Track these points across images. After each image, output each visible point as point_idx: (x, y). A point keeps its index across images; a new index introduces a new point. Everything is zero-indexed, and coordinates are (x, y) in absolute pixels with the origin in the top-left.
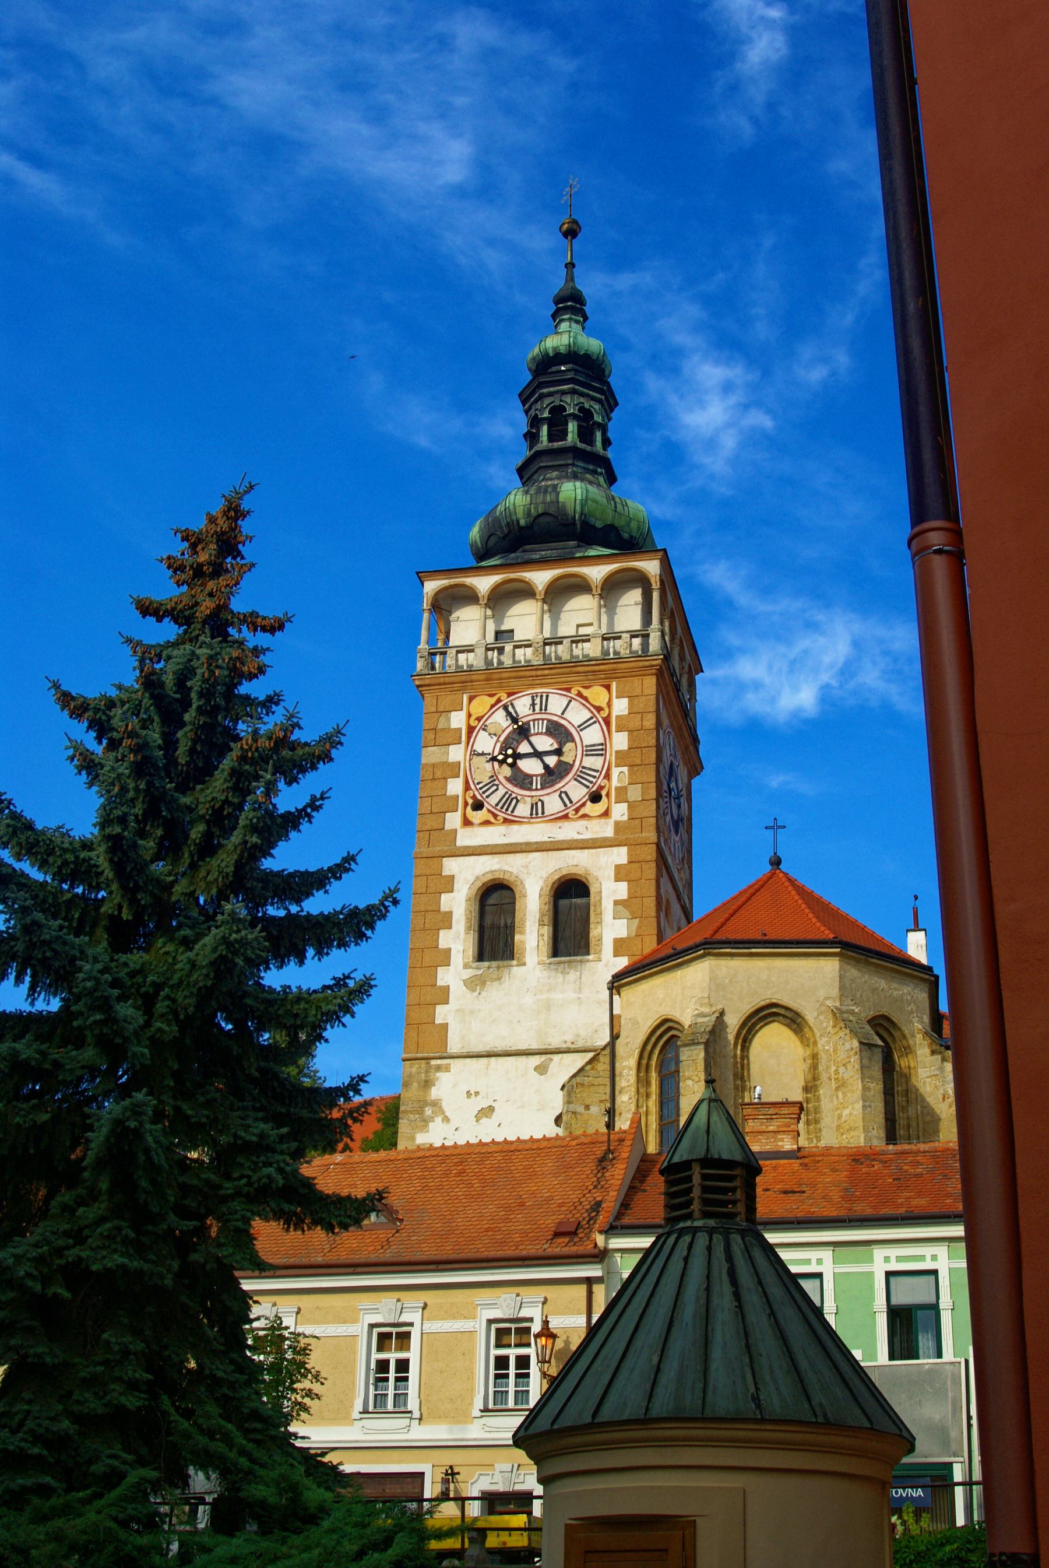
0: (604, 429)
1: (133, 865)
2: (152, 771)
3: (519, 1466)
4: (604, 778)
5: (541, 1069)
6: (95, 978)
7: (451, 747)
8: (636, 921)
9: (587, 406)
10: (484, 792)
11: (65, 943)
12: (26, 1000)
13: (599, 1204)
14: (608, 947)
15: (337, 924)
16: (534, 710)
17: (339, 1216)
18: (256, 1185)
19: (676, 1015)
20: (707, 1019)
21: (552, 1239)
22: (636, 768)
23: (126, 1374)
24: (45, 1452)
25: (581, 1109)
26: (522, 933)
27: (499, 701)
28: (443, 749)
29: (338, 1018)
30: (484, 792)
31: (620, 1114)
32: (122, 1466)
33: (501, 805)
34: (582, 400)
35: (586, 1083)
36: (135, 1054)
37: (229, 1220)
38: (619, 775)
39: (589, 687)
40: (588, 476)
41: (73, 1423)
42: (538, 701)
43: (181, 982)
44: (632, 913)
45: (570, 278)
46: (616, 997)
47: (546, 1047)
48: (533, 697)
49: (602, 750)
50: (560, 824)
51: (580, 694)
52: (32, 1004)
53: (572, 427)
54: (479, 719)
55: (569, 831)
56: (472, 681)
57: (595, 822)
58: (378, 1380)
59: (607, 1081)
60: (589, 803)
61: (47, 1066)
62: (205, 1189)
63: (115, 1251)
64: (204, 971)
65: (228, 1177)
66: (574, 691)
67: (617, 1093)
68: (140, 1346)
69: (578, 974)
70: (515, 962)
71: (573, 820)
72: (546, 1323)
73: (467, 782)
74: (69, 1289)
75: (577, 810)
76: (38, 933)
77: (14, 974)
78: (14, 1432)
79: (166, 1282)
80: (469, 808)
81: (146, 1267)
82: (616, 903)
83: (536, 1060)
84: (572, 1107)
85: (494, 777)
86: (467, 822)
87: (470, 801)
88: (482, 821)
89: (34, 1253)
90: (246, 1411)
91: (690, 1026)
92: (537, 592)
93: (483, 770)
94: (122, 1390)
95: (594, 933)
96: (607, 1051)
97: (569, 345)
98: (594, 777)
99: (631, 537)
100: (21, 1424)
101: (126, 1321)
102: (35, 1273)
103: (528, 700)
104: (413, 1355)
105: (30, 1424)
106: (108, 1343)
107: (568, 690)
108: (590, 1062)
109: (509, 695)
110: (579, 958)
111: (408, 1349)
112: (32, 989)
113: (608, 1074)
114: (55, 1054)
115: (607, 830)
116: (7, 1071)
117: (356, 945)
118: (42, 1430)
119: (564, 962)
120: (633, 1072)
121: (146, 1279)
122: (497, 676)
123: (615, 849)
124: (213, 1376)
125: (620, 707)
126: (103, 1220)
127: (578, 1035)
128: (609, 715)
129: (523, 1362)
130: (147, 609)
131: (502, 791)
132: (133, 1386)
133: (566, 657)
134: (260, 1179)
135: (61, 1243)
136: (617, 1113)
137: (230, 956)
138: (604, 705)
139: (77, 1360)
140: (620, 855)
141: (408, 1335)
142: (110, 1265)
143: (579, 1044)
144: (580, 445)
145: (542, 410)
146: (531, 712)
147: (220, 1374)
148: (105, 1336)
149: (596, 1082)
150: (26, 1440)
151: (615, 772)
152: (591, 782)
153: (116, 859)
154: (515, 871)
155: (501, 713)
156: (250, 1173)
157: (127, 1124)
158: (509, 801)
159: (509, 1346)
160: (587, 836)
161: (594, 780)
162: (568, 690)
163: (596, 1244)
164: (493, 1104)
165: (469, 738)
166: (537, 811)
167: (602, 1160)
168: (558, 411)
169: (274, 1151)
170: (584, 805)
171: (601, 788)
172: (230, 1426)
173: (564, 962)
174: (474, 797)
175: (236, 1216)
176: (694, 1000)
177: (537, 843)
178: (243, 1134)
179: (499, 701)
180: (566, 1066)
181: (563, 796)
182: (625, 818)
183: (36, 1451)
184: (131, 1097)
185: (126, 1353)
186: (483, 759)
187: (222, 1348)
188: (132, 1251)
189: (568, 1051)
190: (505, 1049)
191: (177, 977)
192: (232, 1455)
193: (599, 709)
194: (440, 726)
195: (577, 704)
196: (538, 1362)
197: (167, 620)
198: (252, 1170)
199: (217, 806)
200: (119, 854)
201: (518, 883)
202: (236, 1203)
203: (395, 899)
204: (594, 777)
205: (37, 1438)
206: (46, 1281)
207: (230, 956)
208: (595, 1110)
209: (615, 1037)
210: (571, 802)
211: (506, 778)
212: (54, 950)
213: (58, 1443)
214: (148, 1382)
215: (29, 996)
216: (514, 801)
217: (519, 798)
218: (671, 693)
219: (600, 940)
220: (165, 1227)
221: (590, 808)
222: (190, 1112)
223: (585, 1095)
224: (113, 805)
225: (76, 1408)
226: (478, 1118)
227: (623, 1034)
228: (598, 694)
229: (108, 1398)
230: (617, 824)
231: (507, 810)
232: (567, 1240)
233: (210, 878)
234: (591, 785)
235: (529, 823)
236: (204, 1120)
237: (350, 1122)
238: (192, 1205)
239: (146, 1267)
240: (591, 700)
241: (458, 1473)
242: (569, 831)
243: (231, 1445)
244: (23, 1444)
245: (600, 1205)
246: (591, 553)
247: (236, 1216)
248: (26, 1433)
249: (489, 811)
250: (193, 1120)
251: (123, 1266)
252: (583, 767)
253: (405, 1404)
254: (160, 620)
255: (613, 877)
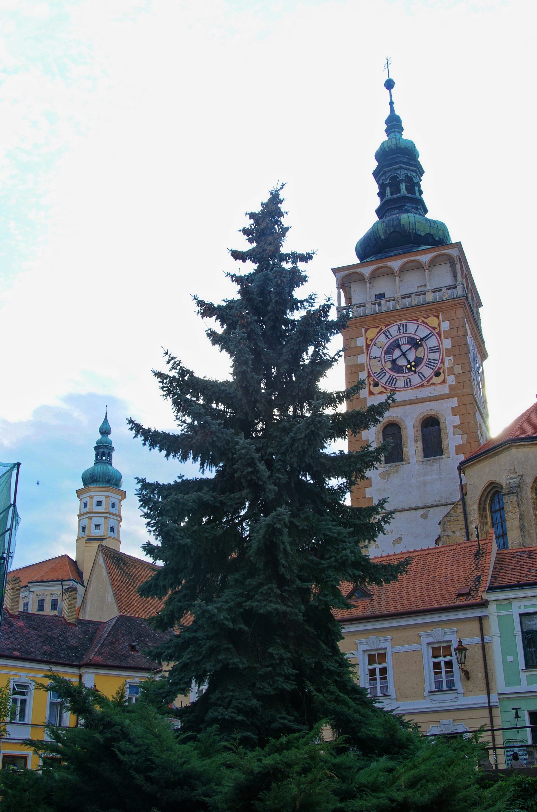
0: (419, 186)
1: (253, 388)
2: (256, 337)
3: (454, 720)
4: (441, 363)
5: (425, 516)
6: (245, 448)
7: (359, 356)
8: (466, 436)
9: (409, 175)
10: (378, 377)
11: (222, 433)
12: (200, 471)
13: (479, 577)
14: (452, 451)
15: (363, 415)
16: (400, 333)
17: (386, 575)
18: (340, 561)
19: (497, 479)
20: (515, 480)
21: (457, 598)
22: (457, 357)
23: (284, 671)
24: (245, 719)
25: (451, 534)
26: (407, 447)
27: (381, 330)
28: (355, 357)
29: (373, 465)
30: (378, 377)
31: (472, 535)
32: (290, 724)
33: (388, 383)
34: (406, 172)
35: (452, 520)
36: (270, 490)
37: (327, 581)
38: (448, 361)
39: (428, 317)
40: (414, 210)
41: (258, 700)
42: (401, 328)
43: (287, 450)
44: (463, 431)
45: (392, 110)
46: (462, 475)
47: (425, 504)
48: (398, 326)
49: (438, 349)
50: (420, 389)
51: (423, 322)
52: (203, 473)
53: (403, 186)
54: (372, 340)
55: (426, 392)
56: (366, 321)
57: (438, 386)
58: (371, 680)
59: (462, 518)
60: (434, 377)
61: (218, 504)
62: (312, 566)
63: (271, 601)
64: (301, 441)
65: (322, 557)
66: (420, 321)
67: (469, 524)
68: (289, 655)
69: (438, 465)
70: (404, 463)
71: (426, 386)
72: (460, 642)
73: (369, 373)
74: (246, 624)
75: (428, 381)
76: (208, 427)
77: (192, 456)
78: (227, 708)
79: (299, 617)
80: (372, 386)
81: (288, 609)
82: (454, 427)
83: (421, 512)
84: (446, 533)
85: (382, 369)
86: (371, 393)
87: (372, 383)
88: (379, 392)
89: (226, 606)
90: (349, 688)
91: (506, 485)
92: (395, 272)
93: (376, 367)
94: (282, 680)
95: (444, 443)
96: (461, 503)
97: (396, 144)
98: (435, 363)
99: (440, 238)
100: (230, 703)
101: (279, 641)
102: (228, 617)
103: (396, 328)
104: (389, 665)
105: (235, 703)
106: (271, 655)
107: (417, 320)
108: (453, 509)
109: (386, 326)
110: (438, 457)
111: (385, 662)
112: (202, 465)
113: (462, 514)
114: (222, 498)
115: (445, 390)
116: (196, 508)
117: (374, 426)
118: (242, 706)
119: (430, 460)
120: (477, 512)
121: (289, 616)
122: (378, 317)
123: (450, 399)
124: (328, 670)
125: (445, 326)
126: (261, 585)
127: (441, 497)
128: (440, 330)
129: (449, 664)
130: (237, 255)
131: (388, 376)
132: (287, 677)
133: (414, 303)
134: (342, 557)
135: (239, 600)
136: (470, 534)
137: (316, 431)
138: (436, 326)
139: (255, 665)
140: (454, 402)
141: (384, 654)
142: (270, 609)
143: (443, 501)
144: (408, 195)
145: (386, 179)
146: (398, 334)
147: (332, 668)
148: (270, 650)
149: (457, 519)
150: (234, 713)
151: (446, 360)
152: (434, 366)
153: (244, 385)
154: (399, 416)
155: (383, 336)
156: (335, 555)
157: (275, 526)
158: (392, 380)
159: (440, 656)
160: (435, 394)
161: (436, 365)
162: (417, 320)
163: (482, 598)
164: (401, 536)
165: (367, 350)
166: (407, 384)
167: (476, 555)
168: (394, 178)
169: (345, 542)
170: (431, 378)
171: (439, 369)
172: (117, 753)
173: (430, 460)
174: (373, 380)
175: (331, 579)
176: (506, 471)
177: (409, 400)
178: (329, 533)
179: (381, 330)
180: (439, 514)
181: (421, 375)
182: (454, 383)
183: (240, 718)
184: (276, 510)
185: (282, 659)
186: (376, 360)
187: (331, 654)
188: (279, 601)
189: (437, 506)
190: (404, 507)
191: (284, 448)
192: (351, 712)
193: (434, 328)
194: (352, 346)
195: (422, 327)
196: (459, 663)
197: (248, 261)
198: (335, 553)
199: (294, 353)
200: (246, 383)
201: (402, 422)
202: (329, 572)
203: (393, 398)
204: (435, 363)
205: (240, 711)
206: (234, 621)
207: (316, 431)
208: (458, 533)
209: (464, 494)
210: (425, 378)
211: (389, 368)
212: (217, 436)
213: (251, 712)
214: (296, 675)
215: (201, 468)
216: (395, 380)
217: (397, 378)
218: (470, 316)
219: (448, 447)
220: (295, 586)
221: (435, 380)
222: (298, 524)
223: (452, 526)
224: (240, 355)
225: (259, 692)
226: (394, 544)
227: (469, 493)
228: (433, 321)
229: (276, 685)
230: (450, 386)
231: (391, 385)
232: (465, 597)
233: (294, 394)
234: (434, 368)
235: (404, 390)
236: (306, 527)
237: (383, 524)
238: (305, 575)
239: (288, 609)
240: (429, 324)
241: (420, 727)
242: (426, 392)
243: (349, 707)
244: (233, 714)
245: (480, 578)
246: (421, 249)
247: (331, 579)
248: (232, 708)
249: (382, 386)
250: (300, 528)
251: (276, 610)
252: (429, 359)
253: (387, 691)
254: (244, 261)
255: (451, 414)
